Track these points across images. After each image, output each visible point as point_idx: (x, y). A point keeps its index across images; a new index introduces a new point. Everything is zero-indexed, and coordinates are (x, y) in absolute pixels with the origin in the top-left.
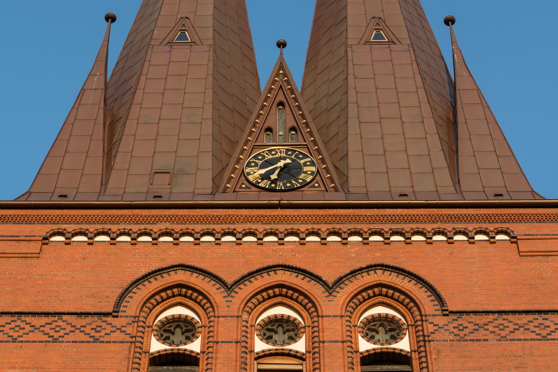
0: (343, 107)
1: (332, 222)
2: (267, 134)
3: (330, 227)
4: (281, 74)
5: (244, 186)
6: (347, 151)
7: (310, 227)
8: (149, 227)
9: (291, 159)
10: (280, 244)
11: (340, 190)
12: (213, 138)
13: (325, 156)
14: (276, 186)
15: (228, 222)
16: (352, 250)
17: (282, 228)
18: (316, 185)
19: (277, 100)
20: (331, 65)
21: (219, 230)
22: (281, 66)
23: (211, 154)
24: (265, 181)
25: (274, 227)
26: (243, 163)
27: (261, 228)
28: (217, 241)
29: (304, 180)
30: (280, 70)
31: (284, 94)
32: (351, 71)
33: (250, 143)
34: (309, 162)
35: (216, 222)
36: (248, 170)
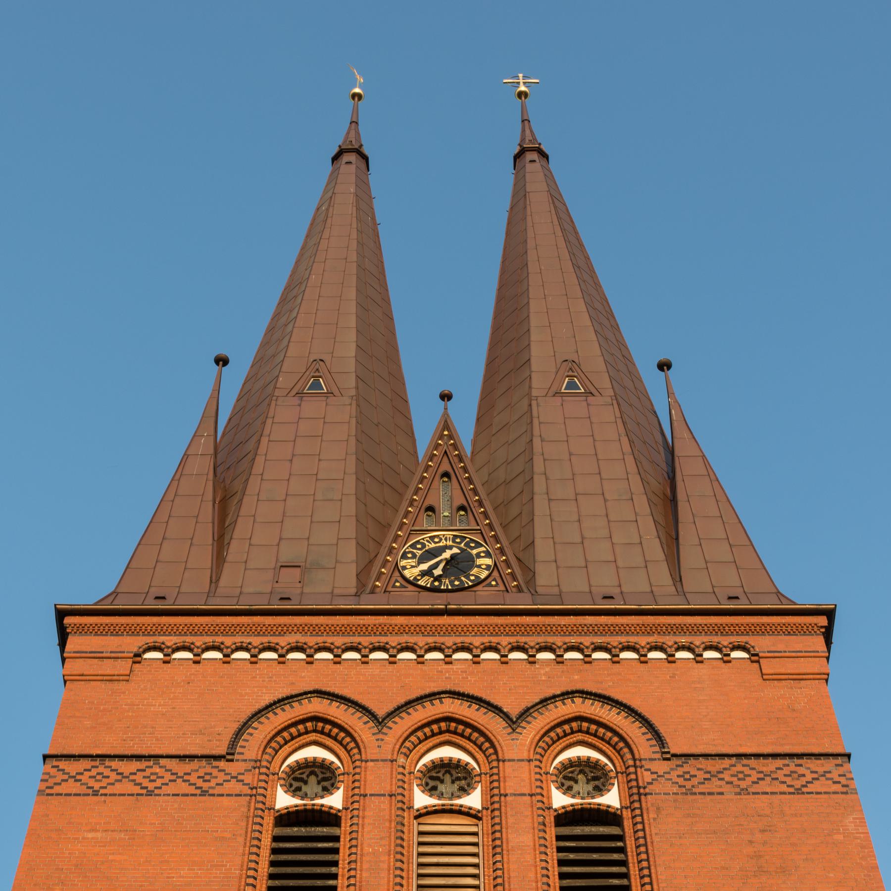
8: (274, 640)
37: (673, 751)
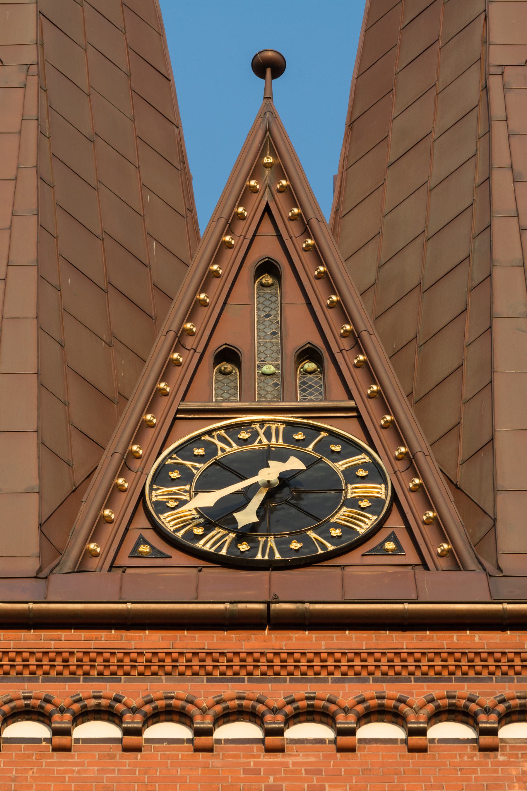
0: (478, 279)
1: (445, 674)
2: (220, 372)
3: (438, 690)
4: (266, 166)
5: (144, 549)
6: (493, 430)
7: (369, 690)
9: (303, 457)
10: (269, 750)
11: (471, 563)
12: (41, 385)
13: (417, 448)
14: (254, 549)
15: (94, 673)
16: (514, 772)
17: (276, 693)
18: (390, 546)
19: (256, 256)
20: (435, 135)
21: (64, 702)
22: (269, 138)
23: (32, 440)
24: (217, 532)
25: (251, 690)
26: (143, 472)
27: (206, 696)
28: (59, 740)
29: (347, 530)
30: (263, 155)
31: (279, 236)
32: (500, 157)
33: (164, 402)
34: (364, 466)
35: (53, 674)
36: (158, 494)
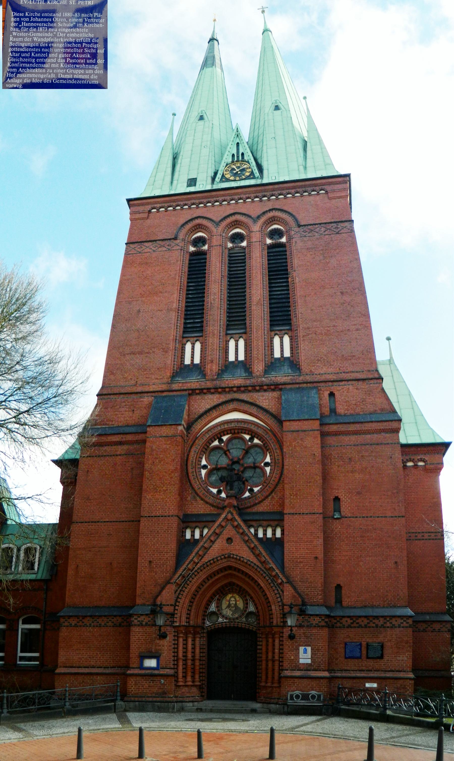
8: (187, 202)
37: (302, 223)
